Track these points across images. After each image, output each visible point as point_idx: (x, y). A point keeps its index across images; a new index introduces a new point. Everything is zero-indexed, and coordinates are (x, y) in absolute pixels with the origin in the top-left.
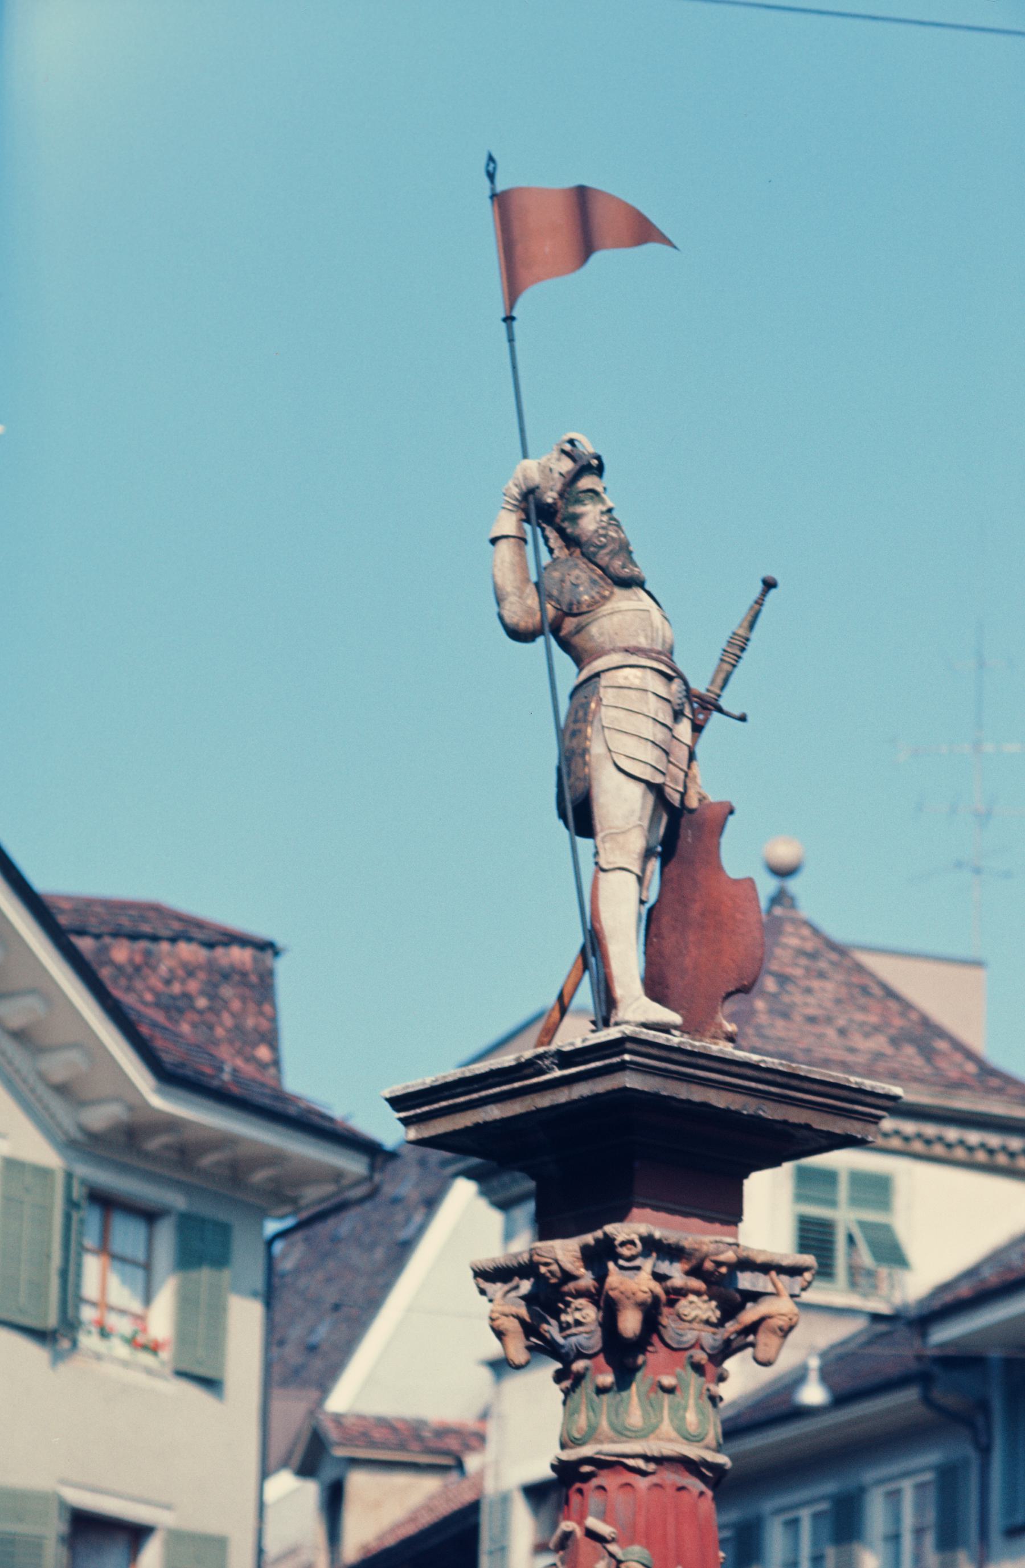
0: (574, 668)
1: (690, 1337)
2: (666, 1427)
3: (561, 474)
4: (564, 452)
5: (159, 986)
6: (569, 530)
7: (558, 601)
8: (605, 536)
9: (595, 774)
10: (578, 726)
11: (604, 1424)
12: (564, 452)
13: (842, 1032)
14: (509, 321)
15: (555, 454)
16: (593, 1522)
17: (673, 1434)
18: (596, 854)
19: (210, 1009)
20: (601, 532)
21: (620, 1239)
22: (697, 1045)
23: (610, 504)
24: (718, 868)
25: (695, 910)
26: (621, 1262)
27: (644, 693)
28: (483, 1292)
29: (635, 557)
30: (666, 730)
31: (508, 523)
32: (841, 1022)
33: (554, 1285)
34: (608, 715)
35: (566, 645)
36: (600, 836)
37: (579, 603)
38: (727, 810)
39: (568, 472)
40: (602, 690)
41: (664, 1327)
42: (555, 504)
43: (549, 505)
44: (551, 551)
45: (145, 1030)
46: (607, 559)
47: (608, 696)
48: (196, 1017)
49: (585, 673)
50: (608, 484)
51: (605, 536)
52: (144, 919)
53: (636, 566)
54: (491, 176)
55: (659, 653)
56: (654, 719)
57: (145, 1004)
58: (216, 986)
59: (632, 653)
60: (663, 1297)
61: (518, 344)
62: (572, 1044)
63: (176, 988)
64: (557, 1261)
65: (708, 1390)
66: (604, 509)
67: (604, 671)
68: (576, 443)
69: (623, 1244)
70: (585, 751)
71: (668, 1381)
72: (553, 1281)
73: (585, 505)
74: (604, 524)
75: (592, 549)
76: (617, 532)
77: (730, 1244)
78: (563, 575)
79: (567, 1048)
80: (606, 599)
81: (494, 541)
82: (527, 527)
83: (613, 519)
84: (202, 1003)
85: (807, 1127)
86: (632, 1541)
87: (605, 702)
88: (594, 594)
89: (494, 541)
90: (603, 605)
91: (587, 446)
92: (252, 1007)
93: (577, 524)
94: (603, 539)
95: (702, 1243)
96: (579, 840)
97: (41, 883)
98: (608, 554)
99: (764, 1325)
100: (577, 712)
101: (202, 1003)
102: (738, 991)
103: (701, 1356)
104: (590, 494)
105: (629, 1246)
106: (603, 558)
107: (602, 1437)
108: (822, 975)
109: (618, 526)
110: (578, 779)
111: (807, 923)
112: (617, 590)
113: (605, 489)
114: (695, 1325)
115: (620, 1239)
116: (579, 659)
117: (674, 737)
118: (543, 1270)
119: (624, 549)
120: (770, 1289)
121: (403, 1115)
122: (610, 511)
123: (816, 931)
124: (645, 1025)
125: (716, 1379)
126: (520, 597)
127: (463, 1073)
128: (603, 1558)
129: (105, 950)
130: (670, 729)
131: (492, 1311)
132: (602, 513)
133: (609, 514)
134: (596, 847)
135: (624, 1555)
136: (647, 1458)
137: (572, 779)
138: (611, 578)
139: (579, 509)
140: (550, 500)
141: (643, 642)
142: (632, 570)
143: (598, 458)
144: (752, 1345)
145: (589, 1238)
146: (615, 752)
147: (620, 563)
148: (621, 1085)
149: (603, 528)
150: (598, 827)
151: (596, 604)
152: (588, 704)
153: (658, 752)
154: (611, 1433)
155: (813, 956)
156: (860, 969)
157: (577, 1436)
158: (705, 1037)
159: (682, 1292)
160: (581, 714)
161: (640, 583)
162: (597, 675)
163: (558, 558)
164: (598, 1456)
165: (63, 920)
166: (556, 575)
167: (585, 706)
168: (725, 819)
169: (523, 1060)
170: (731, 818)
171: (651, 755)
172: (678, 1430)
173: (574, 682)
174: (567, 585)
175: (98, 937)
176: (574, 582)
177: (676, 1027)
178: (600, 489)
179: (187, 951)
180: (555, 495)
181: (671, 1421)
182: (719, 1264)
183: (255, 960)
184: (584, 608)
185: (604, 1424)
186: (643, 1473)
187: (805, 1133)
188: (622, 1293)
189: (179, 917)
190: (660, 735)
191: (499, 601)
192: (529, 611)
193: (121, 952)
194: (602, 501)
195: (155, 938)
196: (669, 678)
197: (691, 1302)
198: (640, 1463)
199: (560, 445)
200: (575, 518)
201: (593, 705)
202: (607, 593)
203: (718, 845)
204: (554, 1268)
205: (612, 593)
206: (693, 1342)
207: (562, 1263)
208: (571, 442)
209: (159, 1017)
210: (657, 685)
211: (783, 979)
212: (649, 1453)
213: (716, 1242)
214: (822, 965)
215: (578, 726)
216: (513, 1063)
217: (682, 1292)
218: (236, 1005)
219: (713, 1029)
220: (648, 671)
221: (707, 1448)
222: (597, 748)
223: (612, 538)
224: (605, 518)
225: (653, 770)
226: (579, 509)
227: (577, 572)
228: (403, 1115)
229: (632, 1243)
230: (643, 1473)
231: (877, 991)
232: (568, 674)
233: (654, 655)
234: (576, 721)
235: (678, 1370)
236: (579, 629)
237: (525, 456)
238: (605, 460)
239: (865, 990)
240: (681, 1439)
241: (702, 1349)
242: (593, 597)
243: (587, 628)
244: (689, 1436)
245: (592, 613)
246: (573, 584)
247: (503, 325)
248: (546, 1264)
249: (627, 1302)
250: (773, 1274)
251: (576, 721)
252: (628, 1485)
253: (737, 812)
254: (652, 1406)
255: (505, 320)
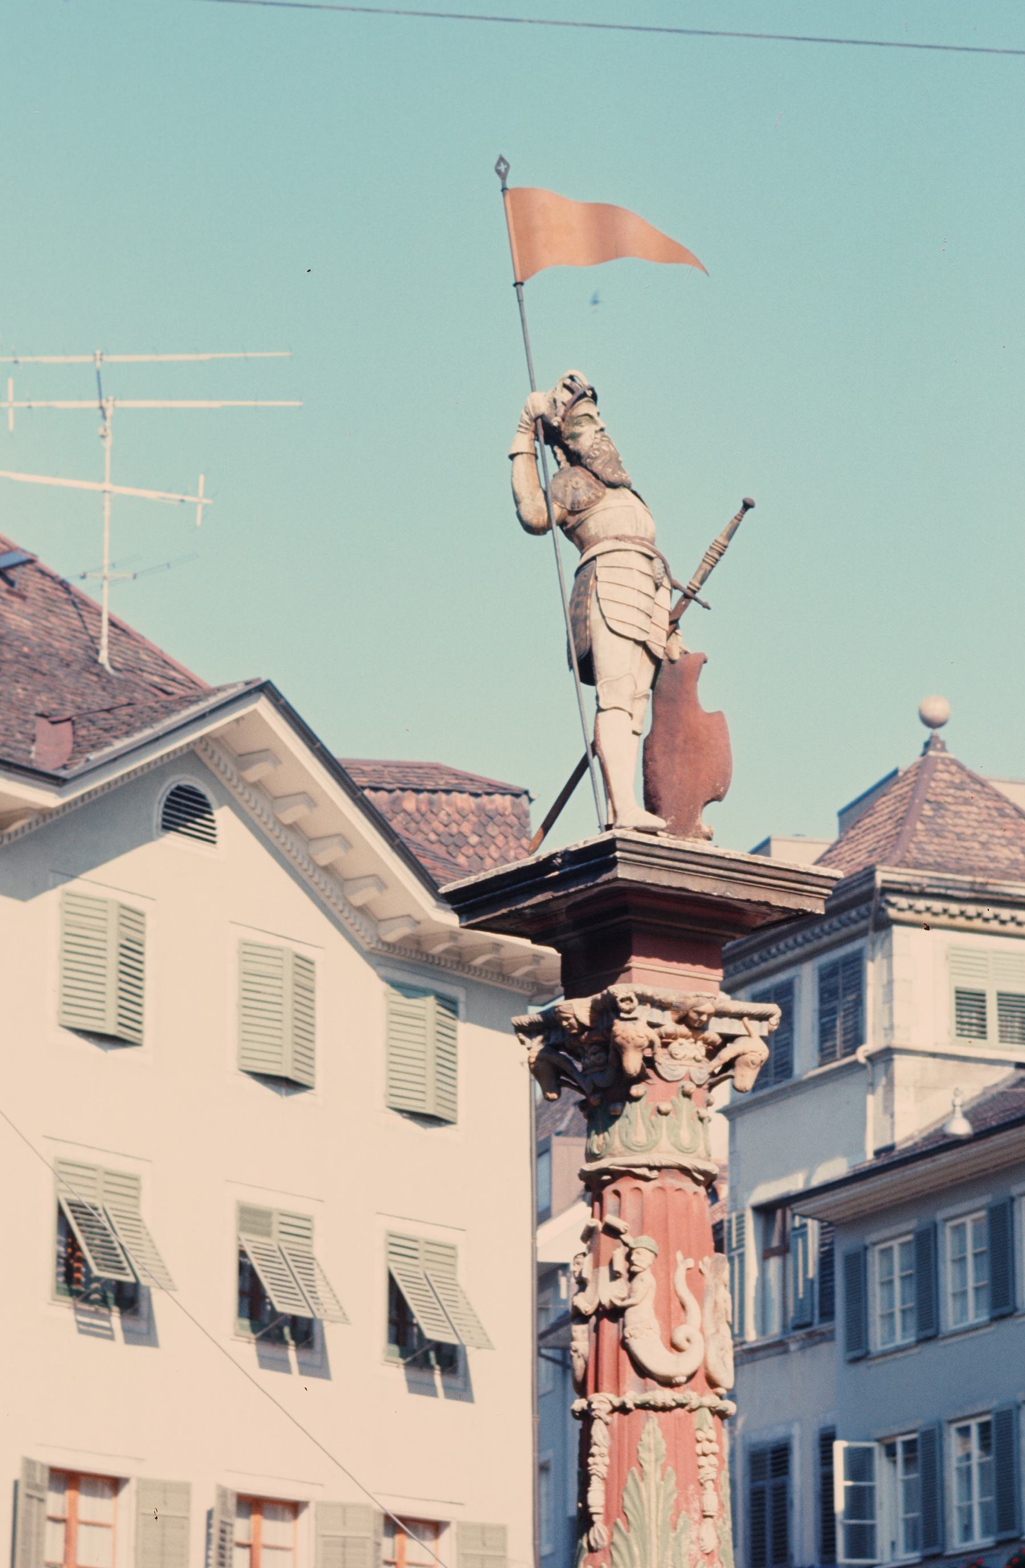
0: (578, 553)
1: (681, 1071)
2: (665, 1143)
3: (564, 403)
4: (565, 386)
5: (441, 829)
6: (571, 447)
7: (563, 502)
8: (598, 450)
9: (594, 635)
10: (580, 599)
11: (617, 1143)
12: (565, 386)
13: (983, 844)
14: (519, 286)
15: (559, 386)
16: (611, 1219)
17: (671, 1148)
18: (597, 698)
19: (481, 843)
20: (595, 446)
21: (620, 996)
22: (687, 844)
23: (602, 425)
24: (696, 705)
25: (679, 740)
26: (622, 1015)
27: (630, 571)
28: (522, 1042)
29: (623, 465)
30: (648, 599)
31: (523, 442)
32: (983, 838)
33: (575, 1034)
34: (603, 589)
35: (571, 533)
36: (599, 684)
37: (579, 503)
38: (702, 660)
39: (569, 401)
40: (598, 570)
41: (660, 1064)
42: (559, 427)
43: (554, 428)
44: (559, 463)
45: (425, 862)
46: (600, 467)
47: (601, 573)
48: (471, 851)
49: (586, 557)
50: (603, 411)
51: (598, 450)
52: (430, 777)
53: (625, 472)
54: (503, 176)
55: (643, 539)
56: (639, 591)
57: (432, 843)
58: (485, 826)
59: (620, 540)
60: (658, 1042)
61: (525, 304)
62: (576, 845)
63: (454, 829)
64: (575, 1017)
65: (698, 1113)
66: (598, 428)
67: (599, 555)
68: (575, 378)
69: (622, 1000)
70: (586, 618)
71: (664, 1107)
72: (575, 1031)
73: (582, 426)
74: (597, 441)
75: (588, 460)
76: (608, 446)
77: (708, 998)
78: (566, 481)
79: (573, 849)
80: (598, 498)
81: (512, 457)
82: (537, 444)
83: (604, 436)
84: (474, 839)
85: (767, 904)
86: (642, 1233)
87: (599, 579)
88: (590, 495)
89: (512, 457)
90: (598, 503)
91: (584, 380)
92: (513, 843)
93: (578, 442)
94: (596, 452)
95: (686, 997)
96: (584, 686)
97: (338, 752)
98: (601, 463)
99: (740, 1059)
100: (579, 587)
101: (474, 839)
102: (713, 800)
103: (690, 1087)
104: (587, 417)
105: (628, 1002)
106: (597, 467)
107: (616, 1152)
108: (967, 802)
109: (609, 441)
110: (582, 639)
111: (954, 762)
112: (609, 491)
113: (598, 414)
114: (683, 1062)
115: (620, 996)
116: (582, 545)
117: (655, 603)
118: (565, 1023)
119: (615, 461)
120: (744, 1032)
121: (455, 906)
122: (602, 430)
123: (961, 768)
124: (638, 830)
125: (705, 1105)
126: (533, 500)
127: (497, 871)
128: (619, 1247)
129: (396, 801)
130: (653, 599)
131: (530, 1057)
132: (596, 432)
133: (602, 433)
134: (597, 693)
135: (635, 1243)
136: (651, 1168)
137: (577, 641)
138: (604, 482)
139: (577, 429)
140: (555, 424)
141: (629, 532)
142: (621, 475)
143: (592, 389)
144: (732, 1077)
145: (598, 996)
146: (13, 567)
147: (610, 470)
148: (615, 876)
149: (597, 444)
150: (598, 677)
151: (591, 503)
152: (588, 582)
153: (643, 617)
154: (622, 1149)
155: (960, 787)
156: (998, 796)
157: (596, 1151)
158: (689, 837)
159: (674, 1037)
160: (582, 589)
161: (628, 486)
162: (594, 558)
163: (563, 468)
164: (612, 1167)
165: (359, 780)
166: (561, 482)
167: (585, 584)
168: (701, 667)
169: (541, 859)
170: (704, 666)
171: (641, 620)
172: (674, 1145)
173: (579, 563)
174: (569, 489)
175: (390, 791)
176: (575, 486)
177: (662, 830)
178: (593, 413)
179: (463, 800)
180: (559, 419)
181: (669, 1137)
182: (700, 1014)
183: (513, 804)
184: (582, 507)
185: (617, 1143)
186: (646, 1179)
187: (764, 909)
188: (623, 1038)
189: (456, 775)
190: (644, 603)
191: (517, 502)
192: (539, 511)
193: (410, 802)
194: (595, 423)
195: (434, 791)
196: (651, 558)
197: (681, 1044)
198: (645, 1171)
199: (563, 379)
200: (574, 437)
201: (591, 582)
202: (600, 494)
203: (695, 688)
204: (573, 1021)
205: (604, 494)
206: (683, 1075)
207: (578, 1017)
208: (572, 378)
209: (441, 851)
210: (643, 564)
211: (938, 806)
212: (652, 1164)
213: (697, 996)
214: (968, 794)
215: (580, 599)
216: (534, 862)
217: (674, 1037)
218: (500, 840)
219: (694, 831)
220: (633, 553)
221: (699, 1157)
222: (594, 616)
223: (604, 451)
224: (599, 436)
225: (638, 630)
226: (577, 429)
227: (577, 479)
228: (455, 906)
229: (630, 999)
230: (646, 1179)
231: (1009, 811)
232: (571, 556)
233: (638, 541)
234: (579, 595)
235: (673, 1098)
236: (581, 523)
237: (533, 389)
238: (597, 391)
239: (1003, 815)
240: (678, 1152)
241: (691, 1080)
242: (589, 498)
243: (587, 522)
244: (682, 1149)
245: (586, 512)
246: (574, 488)
247: (514, 289)
248: (567, 1019)
249: (628, 1045)
250: (746, 1019)
251: (579, 595)
252: (638, 1189)
253: (709, 661)
254: (653, 1126)
255: (515, 285)
